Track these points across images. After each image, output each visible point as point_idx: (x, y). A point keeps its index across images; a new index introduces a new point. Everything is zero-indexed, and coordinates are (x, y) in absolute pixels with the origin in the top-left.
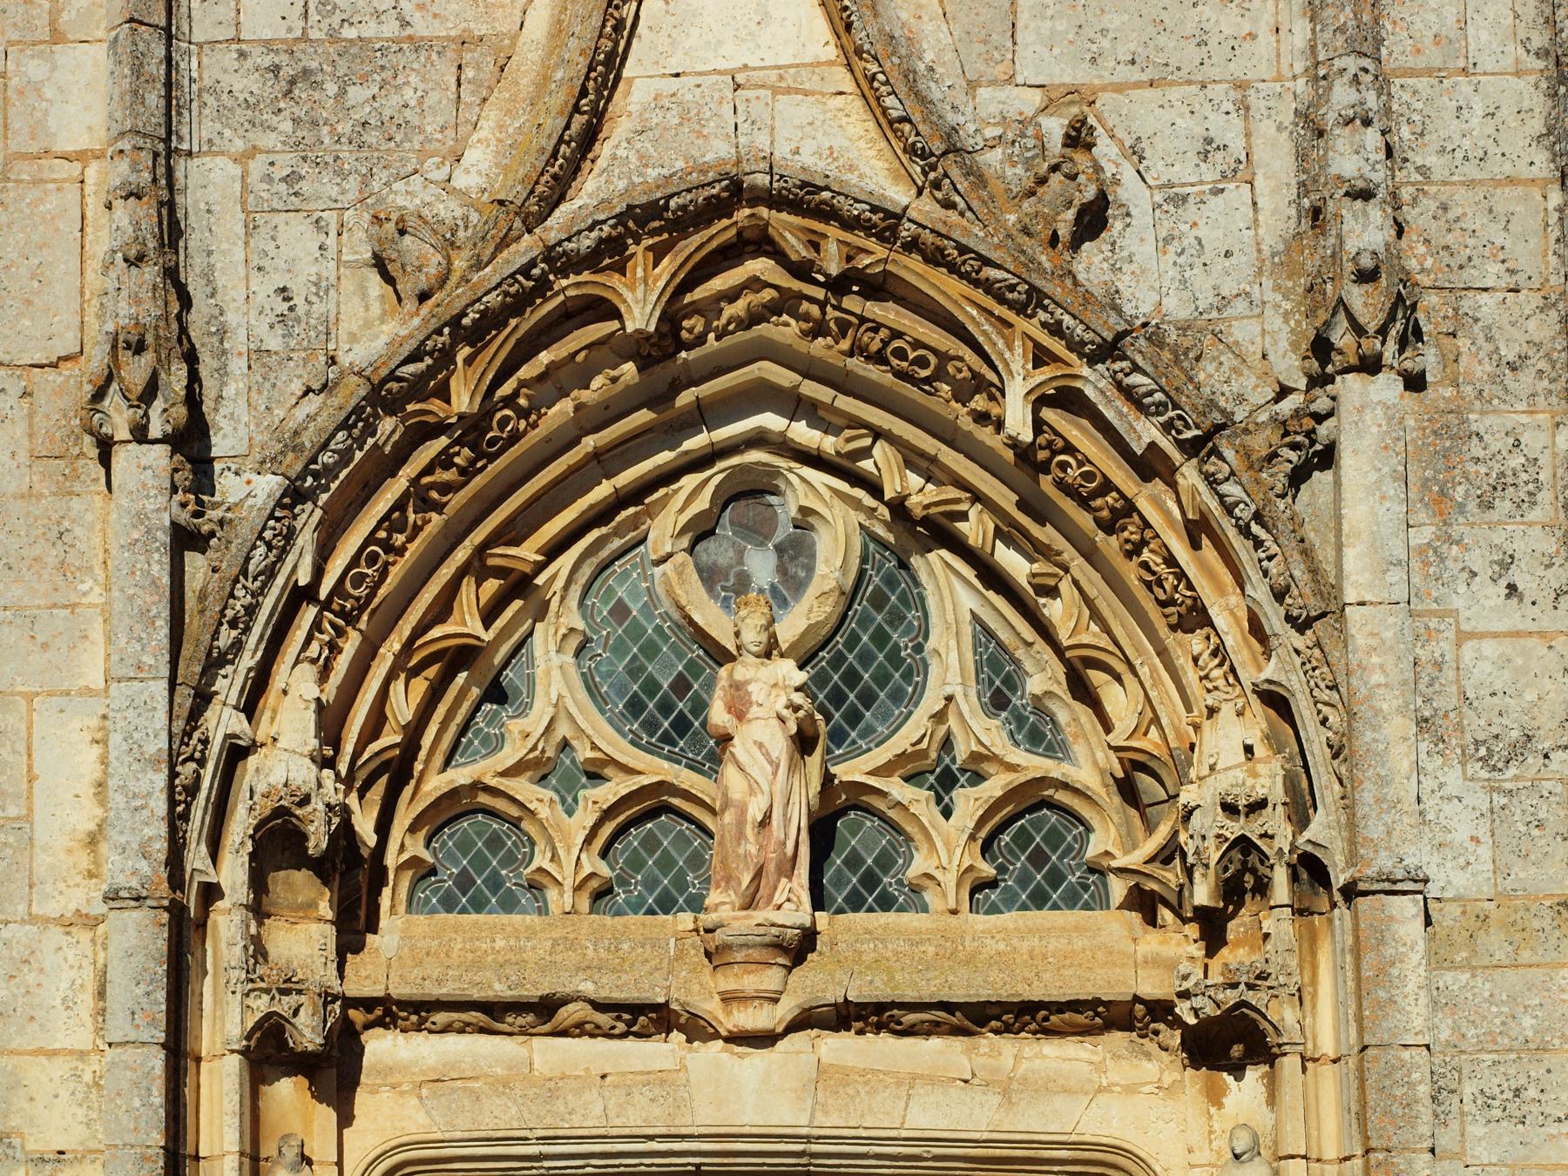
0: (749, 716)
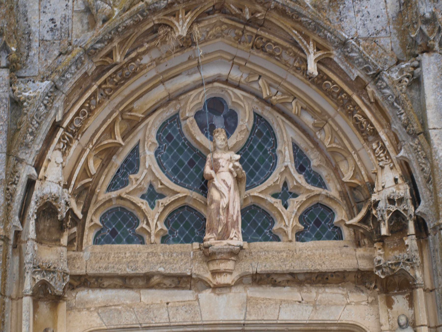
0: (220, 171)
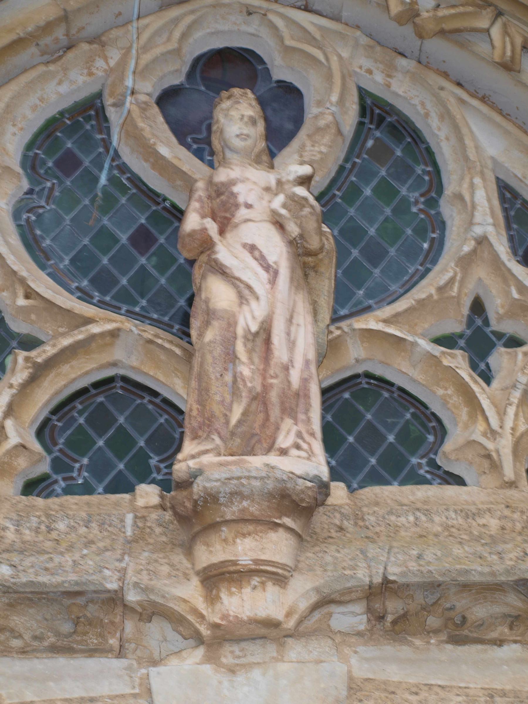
0: (236, 220)
